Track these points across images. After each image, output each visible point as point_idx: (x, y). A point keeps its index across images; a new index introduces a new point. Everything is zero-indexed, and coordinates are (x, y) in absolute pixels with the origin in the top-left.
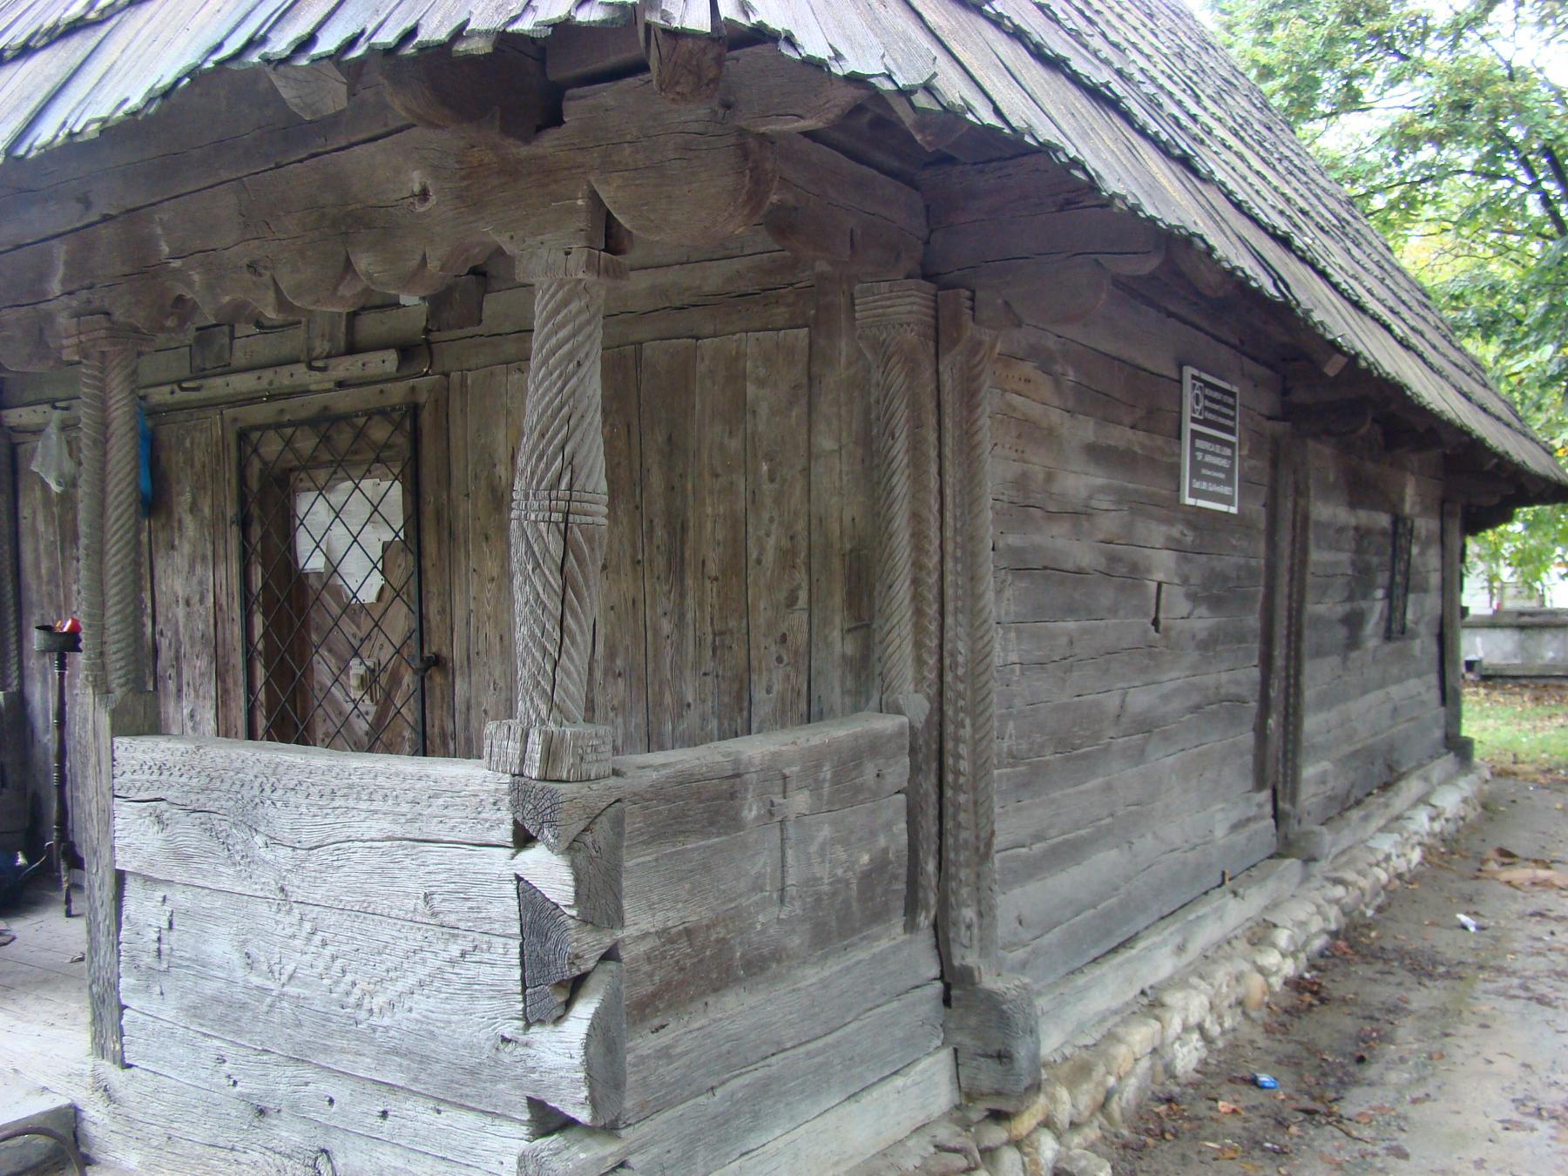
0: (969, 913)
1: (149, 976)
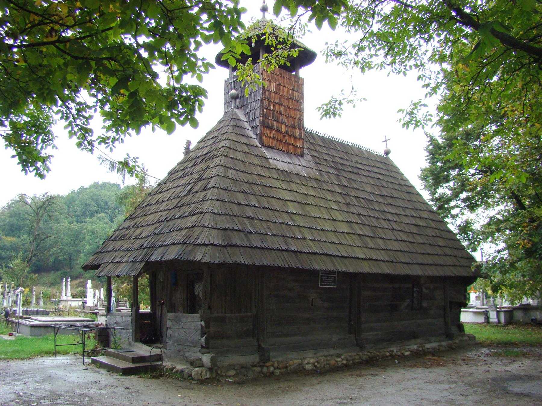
1: (170, 338)
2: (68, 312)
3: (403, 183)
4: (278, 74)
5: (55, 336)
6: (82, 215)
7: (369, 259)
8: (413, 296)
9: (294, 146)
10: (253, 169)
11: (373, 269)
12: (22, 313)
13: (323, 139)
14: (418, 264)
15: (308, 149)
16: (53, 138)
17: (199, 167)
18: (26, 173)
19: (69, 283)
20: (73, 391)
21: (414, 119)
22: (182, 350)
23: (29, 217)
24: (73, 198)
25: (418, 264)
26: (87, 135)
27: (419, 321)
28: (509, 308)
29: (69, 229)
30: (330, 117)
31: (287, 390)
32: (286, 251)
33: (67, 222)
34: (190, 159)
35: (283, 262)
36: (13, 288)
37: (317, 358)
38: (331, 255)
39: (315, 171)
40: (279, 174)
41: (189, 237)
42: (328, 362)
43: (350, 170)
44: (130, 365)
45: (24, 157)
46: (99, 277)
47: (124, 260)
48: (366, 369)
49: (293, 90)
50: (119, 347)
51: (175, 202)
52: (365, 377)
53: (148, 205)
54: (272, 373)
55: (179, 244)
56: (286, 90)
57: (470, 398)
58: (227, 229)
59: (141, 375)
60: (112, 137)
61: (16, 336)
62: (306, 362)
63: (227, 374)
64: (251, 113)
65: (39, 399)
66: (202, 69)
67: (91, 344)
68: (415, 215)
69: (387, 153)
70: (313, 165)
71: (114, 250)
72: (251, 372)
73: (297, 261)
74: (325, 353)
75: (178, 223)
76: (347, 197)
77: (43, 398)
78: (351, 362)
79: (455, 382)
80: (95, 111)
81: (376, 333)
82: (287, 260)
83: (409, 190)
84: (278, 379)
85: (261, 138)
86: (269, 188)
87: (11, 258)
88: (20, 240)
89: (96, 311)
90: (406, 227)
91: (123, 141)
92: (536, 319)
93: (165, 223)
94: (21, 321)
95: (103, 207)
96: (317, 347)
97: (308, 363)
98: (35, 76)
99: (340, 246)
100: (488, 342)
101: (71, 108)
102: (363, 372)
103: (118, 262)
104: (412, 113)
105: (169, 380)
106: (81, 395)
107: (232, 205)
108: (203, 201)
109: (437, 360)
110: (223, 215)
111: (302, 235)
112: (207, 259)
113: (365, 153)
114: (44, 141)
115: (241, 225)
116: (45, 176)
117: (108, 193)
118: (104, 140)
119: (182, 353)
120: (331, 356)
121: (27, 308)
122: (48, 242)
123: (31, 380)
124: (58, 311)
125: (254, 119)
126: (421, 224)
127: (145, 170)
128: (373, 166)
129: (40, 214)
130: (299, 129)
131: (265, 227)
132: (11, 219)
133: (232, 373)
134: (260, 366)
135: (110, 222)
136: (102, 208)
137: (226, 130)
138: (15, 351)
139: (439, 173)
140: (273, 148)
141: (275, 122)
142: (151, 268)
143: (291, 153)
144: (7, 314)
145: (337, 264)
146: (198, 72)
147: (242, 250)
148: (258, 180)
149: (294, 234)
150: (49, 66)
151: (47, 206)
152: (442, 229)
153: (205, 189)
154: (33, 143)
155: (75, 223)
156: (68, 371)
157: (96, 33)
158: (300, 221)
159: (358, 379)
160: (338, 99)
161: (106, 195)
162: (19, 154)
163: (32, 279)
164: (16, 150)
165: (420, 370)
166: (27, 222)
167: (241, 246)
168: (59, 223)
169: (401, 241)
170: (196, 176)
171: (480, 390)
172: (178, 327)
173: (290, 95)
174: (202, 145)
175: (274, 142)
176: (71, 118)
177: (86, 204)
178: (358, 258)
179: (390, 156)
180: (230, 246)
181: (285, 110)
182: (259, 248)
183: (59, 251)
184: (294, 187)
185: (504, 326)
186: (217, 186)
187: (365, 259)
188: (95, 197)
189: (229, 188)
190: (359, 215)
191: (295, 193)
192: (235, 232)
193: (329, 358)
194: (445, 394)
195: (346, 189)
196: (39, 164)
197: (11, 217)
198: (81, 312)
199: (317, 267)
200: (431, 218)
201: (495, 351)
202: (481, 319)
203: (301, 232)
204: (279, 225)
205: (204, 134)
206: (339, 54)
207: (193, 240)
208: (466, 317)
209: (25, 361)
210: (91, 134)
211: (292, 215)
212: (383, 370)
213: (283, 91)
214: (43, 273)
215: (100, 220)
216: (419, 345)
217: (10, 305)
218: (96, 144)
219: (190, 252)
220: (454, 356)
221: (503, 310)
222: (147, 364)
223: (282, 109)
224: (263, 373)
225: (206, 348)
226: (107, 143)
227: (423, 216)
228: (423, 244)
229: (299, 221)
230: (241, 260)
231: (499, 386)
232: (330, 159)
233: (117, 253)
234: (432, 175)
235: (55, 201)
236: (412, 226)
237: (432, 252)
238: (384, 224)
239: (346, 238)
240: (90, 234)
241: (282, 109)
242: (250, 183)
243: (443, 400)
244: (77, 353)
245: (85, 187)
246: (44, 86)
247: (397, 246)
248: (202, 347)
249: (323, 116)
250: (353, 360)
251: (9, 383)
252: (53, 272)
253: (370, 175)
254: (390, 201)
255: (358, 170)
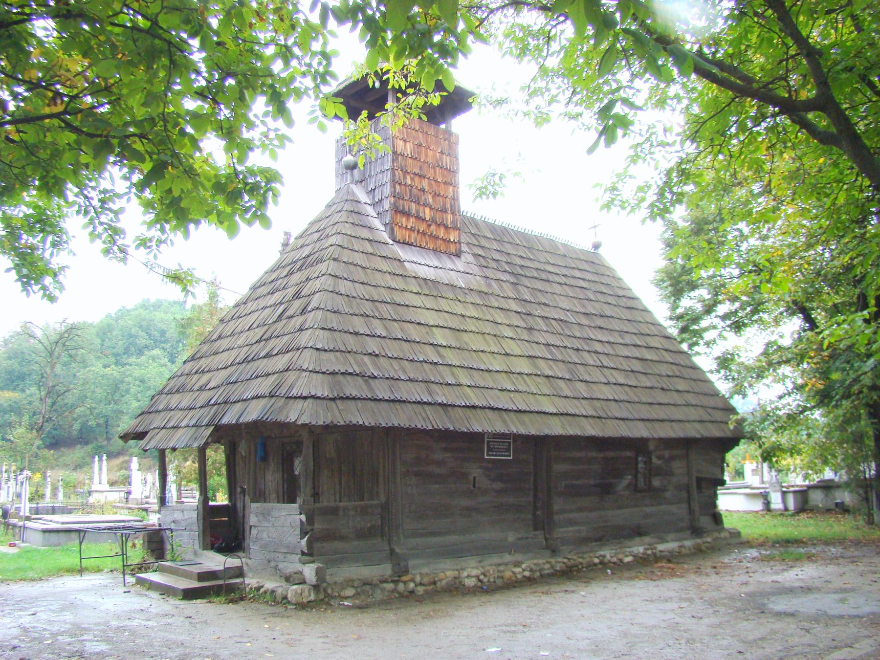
0: (395, 538)
2: (102, 509)
3: (621, 293)
4: (417, 128)
5: (81, 543)
6: (124, 354)
7: (562, 414)
8: (636, 469)
9: (444, 240)
10: (379, 279)
11: (568, 428)
12: (30, 511)
13: (492, 228)
14: (642, 420)
15: (468, 244)
16: (69, 238)
17: (296, 278)
18: (28, 295)
19: (105, 463)
20: (107, 624)
21: (619, 198)
22: (274, 560)
23: (37, 359)
24: (109, 325)
25: (642, 420)
26: (117, 237)
27: (648, 510)
28: (802, 486)
29: (103, 376)
30: (488, 198)
31: (431, 616)
32: (430, 404)
33: (101, 365)
34: (283, 264)
35: (424, 420)
36: (14, 472)
37: (483, 567)
38: (501, 409)
39: (478, 278)
40: (420, 285)
41: (279, 386)
42: (500, 574)
43: (536, 275)
44: (195, 584)
45: (25, 271)
46: (146, 451)
47: (183, 424)
48: (558, 584)
49: (442, 153)
50: (179, 559)
51: (259, 332)
52: (555, 595)
53: (220, 337)
54: (412, 592)
55: (263, 397)
56: (431, 153)
57: (706, 621)
58: (337, 373)
59: (212, 599)
60: (156, 238)
61: (20, 547)
62: (465, 574)
63: (342, 594)
64: (377, 191)
65: (54, 635)
66: (276, 143)
67: (137, 553)
68: (639, 343)
69: (596, 246)
70: (476, 270)
71: (168, 409)
72: (379, 591)
73: (446, 419)
74: (496, 559)
75: (263, 366)
76: (529, 318)
77: (62, 634)
78: (538, 574)
79: (690, 600)
80: (129, 200)
81: (577, 528)
82: (431, 418)
83: (631, 305)
84: (420, 600)
85: (392, 230)
86: (405, 308)
87: (10, 425)
88: (24, 395)
89: (146, 506)
90: (624, 364)
91: (172, 243)
92: (842, 503)
93: (244, 365)
94: (28, 524)
95: (159, 338)
96: (482, 550)
97: (468, 576)
98: (34, 158)
99: (516, 394)
100: (761, 540)
101: (92, 198)
102: (554, 588)
103: (173, 428)
104: (614, 189)
105: (253, 605)
106: (118, 628)
107: (345, 335)
108: (301, 330)
109: (673, 569)
110: (331, 351)
111: (455, 378)
112: (305, 419)
113: (561, 248)
114: (54, 245)
115: (359, 366)
116: (57, 298)
117: (166, 317)
118: (144, 243)
119: (273, 564)
120: (506, 564)
121: (38, 504)
122: (70, 399)
123: (43, 608)
124: (87, 508)
125: (381, 200)
126: (649, 358)
127: (218, 281)
128: (574, 268)
129: (56, 354)
130: (453, 213)
131: (397, 368)
132: (10, 362)
133: (350, 592)
134: (393, 581)
135: (169, 364)
136: (156, 341)
137: (336, 218)
138: (19, 569)
139: (680, 275)
140: (411, 245)
141: (413, 205)
142: (224, 434)
143: (440, 251)
144: (5, 514)
145: (509, 423)
146: (271, 147)
147: (359, 403)
148: (386, 296)
149: (443, 378)
150: (54, 143)
151: (66, 342)
152: (683, 364)
153: (303, 312)
154: (38, 249)
155: (113, 366)
156: (102, 598)
157: (119, 99)
158: (452, 357)
159: (544, 597)
160: (499, 172)
161: (162, 320)
162: (17, 267)
163: (45, 459)
164: (13, 261)
165: (641, 583)
166: (36, 367)
167: (359, 399)
168: (85, 367)
169: (615, 384)
170: (291, 291)
171: (722, 609)
172: (266, 524)
173: (437, 162)
174: (301, 242)
175: (414, 235)
176: (92, 213)
177: (131, 336)
178: (545, 413)
179: (600, 251)
180: (341, 398)
181: (430, 185)
182: (386, 401)
183: (88, 412)
184: (444, 305)
185: (793, 515)
186: (322, 306)
187: (555, 414)
188: (144, 324)
189: (341, 309)
190: (548, 345)
191: (446, 314)
192: (349, 378)
193: (501, 568)
194: (670, 615)
195: (528, 305)
196: (48, 280)
197: (10, 358)
198: (123, 508)
199: (477, 428)
200: (666, 347)
201: (768, 553)
202: (758, 505)
203: (453, 374)
204: (418, 364)
205: (305, 226)
206: (500, 102)
207: (284, 392)
208: (729, 502)
209: (35, 583)
210: (122, 236)
211: (440, 348)
212: (584, 585)
213: (426, 156)
214: (62, 449)
215: (154, 360)
216: (647, 547)
217: (10, 499)
218: (131, 250)
219: (281, 409)
220: (702, 562)
221: (792, 489)
222: (221, 582)
223: (425, 183)
224: (398, 592)
225: (309, 554)
226: (149, 247)
227: (653, 344)
228: (651, 388)
229: (451, 357)
230: (357, 418)
231: (755, 605)
232: (503, 258)
233: (172, 412)
234: (670, 278)
235: (79, 332)
236: (634, 361)
237: (666, 401)
238: (589, 359)
239: (525, 382)
240: (137, 383)
241: (425, 183)
242: (373, 301)
243: (663, 625)
244: (116, 570)
245: (128, 308)
246: (48, 172)
247: (608, 392)
248: (303, 553)
249: (476, 197)
250: (540, 570)
251: (9, 613)
252: (79, 446)
253: (568, 283)
254: (600, 322)
255: (548, 275)
